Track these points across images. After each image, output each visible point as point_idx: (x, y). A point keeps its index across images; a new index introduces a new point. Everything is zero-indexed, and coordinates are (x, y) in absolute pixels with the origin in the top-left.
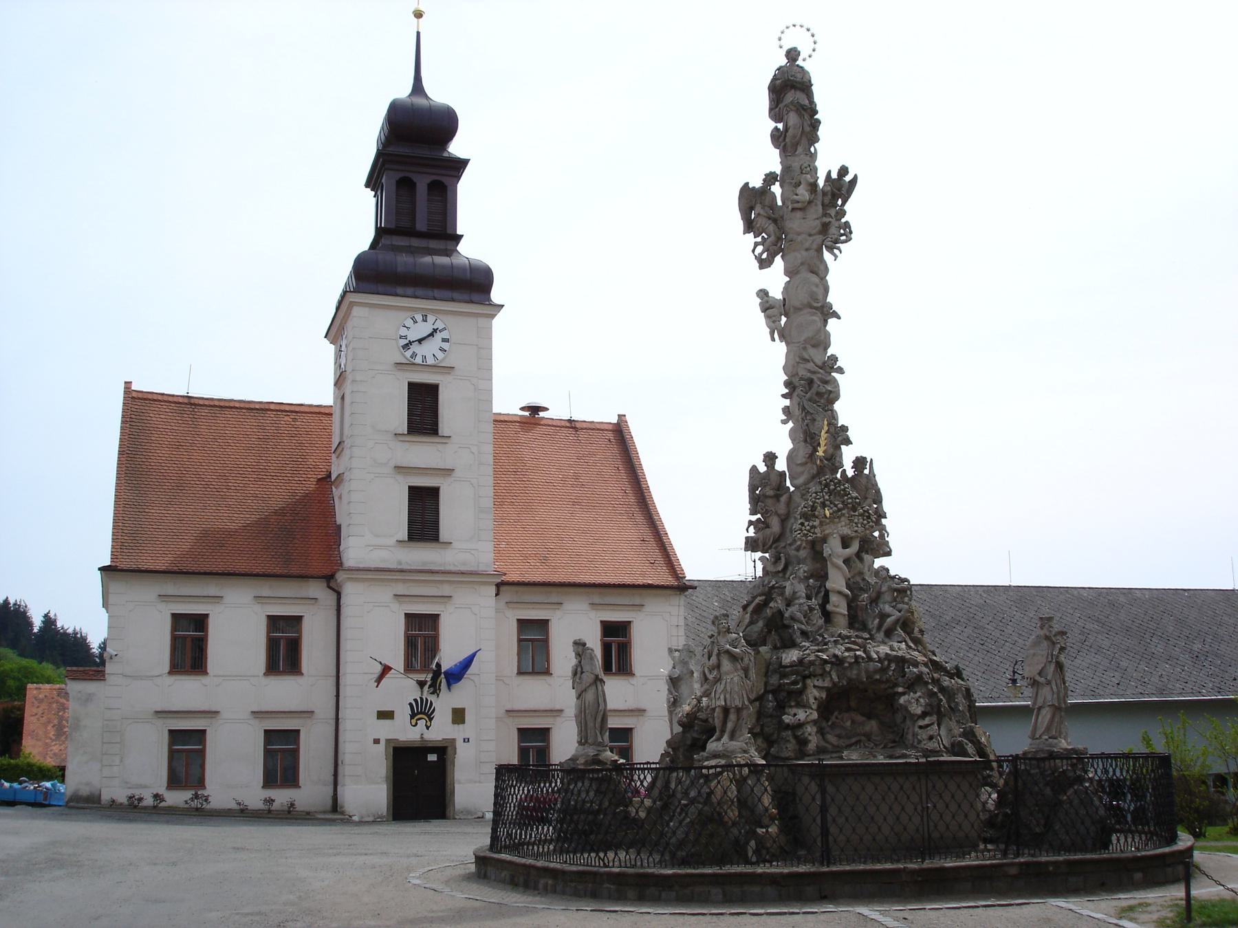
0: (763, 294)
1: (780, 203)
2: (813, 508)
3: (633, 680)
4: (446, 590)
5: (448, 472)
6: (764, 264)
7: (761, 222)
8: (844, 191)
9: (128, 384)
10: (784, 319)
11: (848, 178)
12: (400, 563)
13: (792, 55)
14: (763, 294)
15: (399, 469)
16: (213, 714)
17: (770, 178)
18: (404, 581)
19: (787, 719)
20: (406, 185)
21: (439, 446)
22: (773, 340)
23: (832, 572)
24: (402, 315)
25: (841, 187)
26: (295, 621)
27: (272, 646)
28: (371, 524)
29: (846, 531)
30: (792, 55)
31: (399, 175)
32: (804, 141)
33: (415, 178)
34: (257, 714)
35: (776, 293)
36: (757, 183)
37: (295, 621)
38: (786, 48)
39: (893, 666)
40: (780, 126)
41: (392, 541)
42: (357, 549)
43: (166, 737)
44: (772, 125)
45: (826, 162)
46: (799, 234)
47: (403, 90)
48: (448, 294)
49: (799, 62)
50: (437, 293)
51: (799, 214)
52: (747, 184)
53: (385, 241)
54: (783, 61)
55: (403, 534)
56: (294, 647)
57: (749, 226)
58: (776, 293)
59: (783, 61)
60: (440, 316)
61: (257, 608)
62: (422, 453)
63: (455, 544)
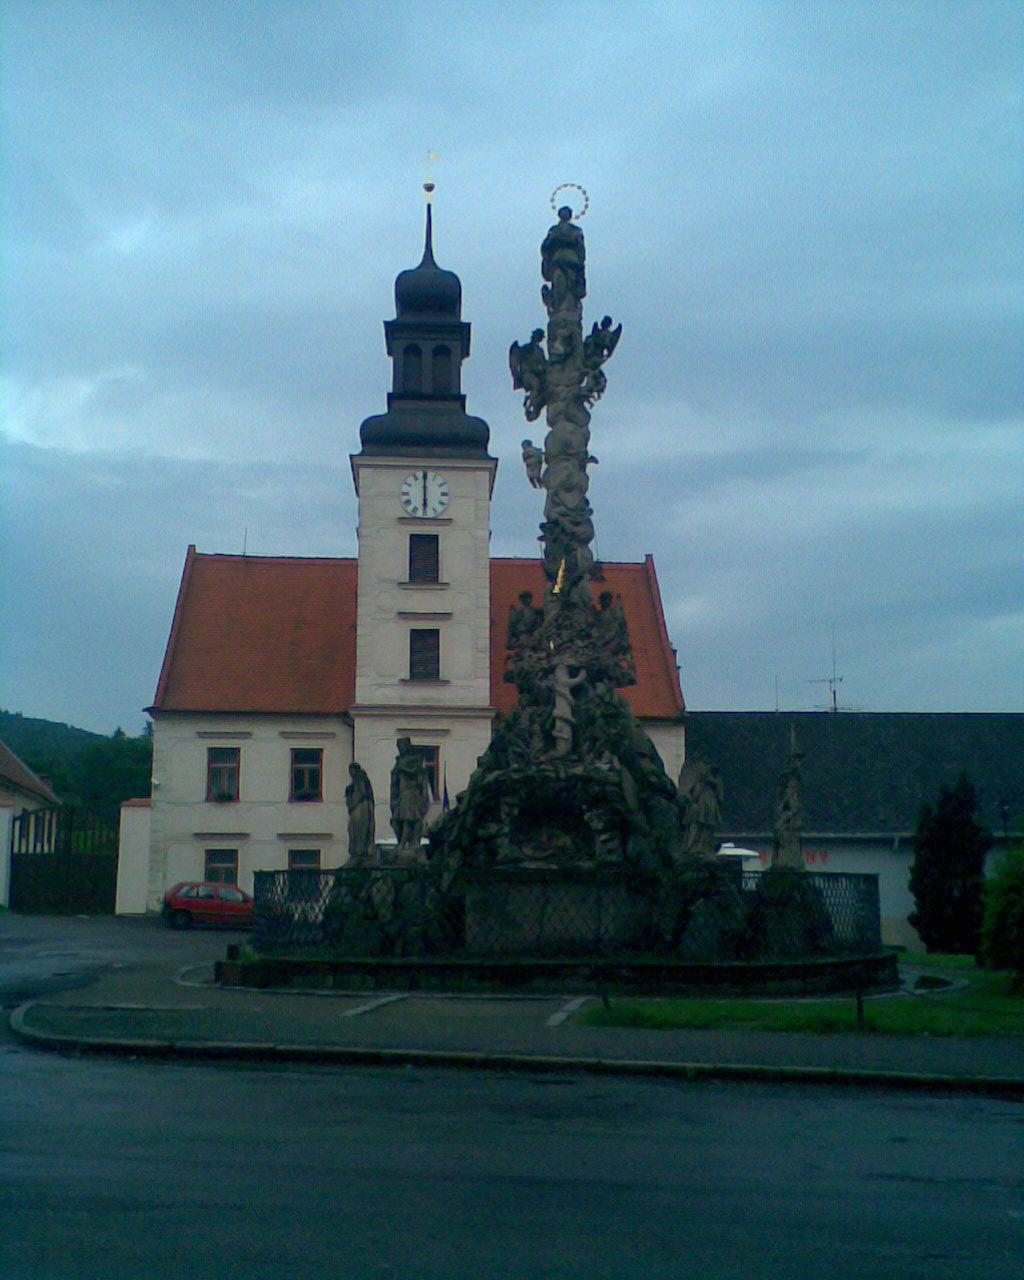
0: (527, 444)
1: (547, 357)
2: (540, 641)
3: (238, 806)
4: (443, 724)
5: (447, 616)
6: (531, 416)
7: (528, 377)
8: (607, 341)
9: (192, 548)
10: (544, 466)
11: (613, 328)
12: (402, 699)
13: (566, 213)
14: (527, 444)
15: (403, 615)
16: (243, 836)
17: (538, 335)
18: (406, 716)
19: (481, 832)
20: (413, 351)
21: (440, 592)
22: (535, 486)
23: (559, 701)
24: (406, 472)
25: (606, 338)
26: (315, 756)
27: (297, 778)
28: (380, 665)
29: (572, 662)
30: (566, 213)
31: (434, 344)
32: (570, 297)
33: (421, 344)
34: (283, 837)
35: (539, 444)
36: (525, 340)
37: (315, 756)
38: (558, 208)
39: (579, 785)
40: (549, 285)
41: (396, 681)
42: (366, 691)
43: (202, 857)
44: (542, 282)
45: (591, 314)
46: (557, 385)
47: (414, 261)
48: (447, 450)
49: (573, 221)
50: (437, 450)
51: (558, 367)
52: (516, 343)
53: (396, 404)
54: (556, 220)
55: (406, 674)
56: (316, 778)
57: (519, 383)
58: (539, 444)
59: (556, 220)
60: (439, 472)
61: (283, 742)
62: (422, 601)
63: (454, 682)
